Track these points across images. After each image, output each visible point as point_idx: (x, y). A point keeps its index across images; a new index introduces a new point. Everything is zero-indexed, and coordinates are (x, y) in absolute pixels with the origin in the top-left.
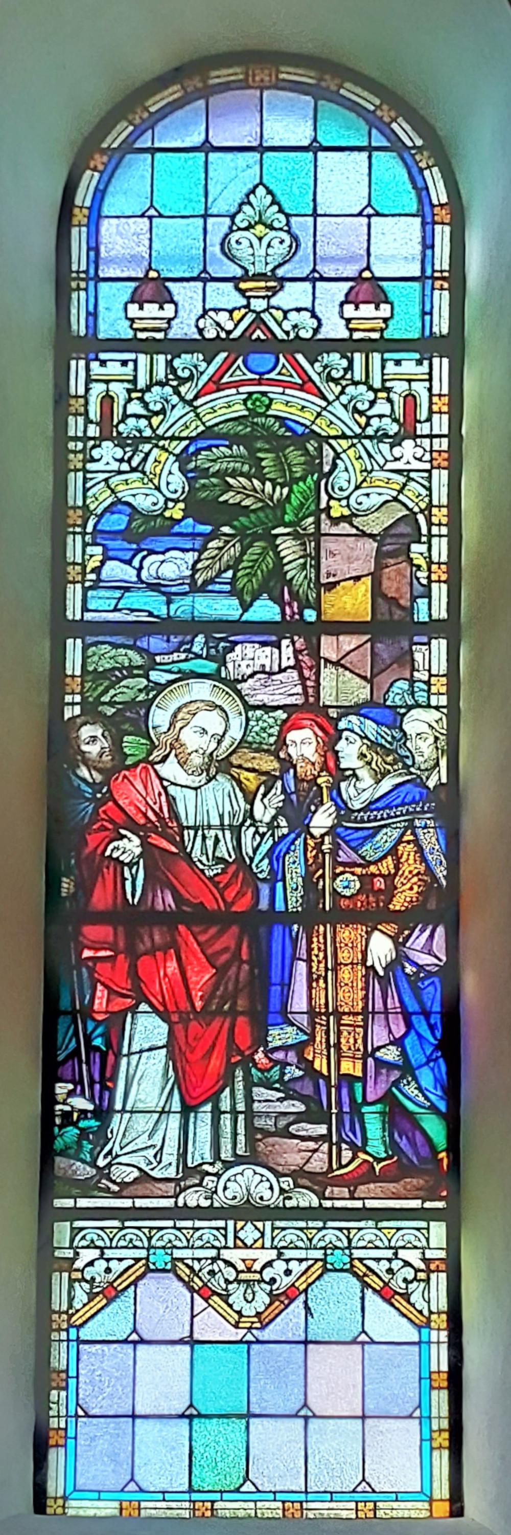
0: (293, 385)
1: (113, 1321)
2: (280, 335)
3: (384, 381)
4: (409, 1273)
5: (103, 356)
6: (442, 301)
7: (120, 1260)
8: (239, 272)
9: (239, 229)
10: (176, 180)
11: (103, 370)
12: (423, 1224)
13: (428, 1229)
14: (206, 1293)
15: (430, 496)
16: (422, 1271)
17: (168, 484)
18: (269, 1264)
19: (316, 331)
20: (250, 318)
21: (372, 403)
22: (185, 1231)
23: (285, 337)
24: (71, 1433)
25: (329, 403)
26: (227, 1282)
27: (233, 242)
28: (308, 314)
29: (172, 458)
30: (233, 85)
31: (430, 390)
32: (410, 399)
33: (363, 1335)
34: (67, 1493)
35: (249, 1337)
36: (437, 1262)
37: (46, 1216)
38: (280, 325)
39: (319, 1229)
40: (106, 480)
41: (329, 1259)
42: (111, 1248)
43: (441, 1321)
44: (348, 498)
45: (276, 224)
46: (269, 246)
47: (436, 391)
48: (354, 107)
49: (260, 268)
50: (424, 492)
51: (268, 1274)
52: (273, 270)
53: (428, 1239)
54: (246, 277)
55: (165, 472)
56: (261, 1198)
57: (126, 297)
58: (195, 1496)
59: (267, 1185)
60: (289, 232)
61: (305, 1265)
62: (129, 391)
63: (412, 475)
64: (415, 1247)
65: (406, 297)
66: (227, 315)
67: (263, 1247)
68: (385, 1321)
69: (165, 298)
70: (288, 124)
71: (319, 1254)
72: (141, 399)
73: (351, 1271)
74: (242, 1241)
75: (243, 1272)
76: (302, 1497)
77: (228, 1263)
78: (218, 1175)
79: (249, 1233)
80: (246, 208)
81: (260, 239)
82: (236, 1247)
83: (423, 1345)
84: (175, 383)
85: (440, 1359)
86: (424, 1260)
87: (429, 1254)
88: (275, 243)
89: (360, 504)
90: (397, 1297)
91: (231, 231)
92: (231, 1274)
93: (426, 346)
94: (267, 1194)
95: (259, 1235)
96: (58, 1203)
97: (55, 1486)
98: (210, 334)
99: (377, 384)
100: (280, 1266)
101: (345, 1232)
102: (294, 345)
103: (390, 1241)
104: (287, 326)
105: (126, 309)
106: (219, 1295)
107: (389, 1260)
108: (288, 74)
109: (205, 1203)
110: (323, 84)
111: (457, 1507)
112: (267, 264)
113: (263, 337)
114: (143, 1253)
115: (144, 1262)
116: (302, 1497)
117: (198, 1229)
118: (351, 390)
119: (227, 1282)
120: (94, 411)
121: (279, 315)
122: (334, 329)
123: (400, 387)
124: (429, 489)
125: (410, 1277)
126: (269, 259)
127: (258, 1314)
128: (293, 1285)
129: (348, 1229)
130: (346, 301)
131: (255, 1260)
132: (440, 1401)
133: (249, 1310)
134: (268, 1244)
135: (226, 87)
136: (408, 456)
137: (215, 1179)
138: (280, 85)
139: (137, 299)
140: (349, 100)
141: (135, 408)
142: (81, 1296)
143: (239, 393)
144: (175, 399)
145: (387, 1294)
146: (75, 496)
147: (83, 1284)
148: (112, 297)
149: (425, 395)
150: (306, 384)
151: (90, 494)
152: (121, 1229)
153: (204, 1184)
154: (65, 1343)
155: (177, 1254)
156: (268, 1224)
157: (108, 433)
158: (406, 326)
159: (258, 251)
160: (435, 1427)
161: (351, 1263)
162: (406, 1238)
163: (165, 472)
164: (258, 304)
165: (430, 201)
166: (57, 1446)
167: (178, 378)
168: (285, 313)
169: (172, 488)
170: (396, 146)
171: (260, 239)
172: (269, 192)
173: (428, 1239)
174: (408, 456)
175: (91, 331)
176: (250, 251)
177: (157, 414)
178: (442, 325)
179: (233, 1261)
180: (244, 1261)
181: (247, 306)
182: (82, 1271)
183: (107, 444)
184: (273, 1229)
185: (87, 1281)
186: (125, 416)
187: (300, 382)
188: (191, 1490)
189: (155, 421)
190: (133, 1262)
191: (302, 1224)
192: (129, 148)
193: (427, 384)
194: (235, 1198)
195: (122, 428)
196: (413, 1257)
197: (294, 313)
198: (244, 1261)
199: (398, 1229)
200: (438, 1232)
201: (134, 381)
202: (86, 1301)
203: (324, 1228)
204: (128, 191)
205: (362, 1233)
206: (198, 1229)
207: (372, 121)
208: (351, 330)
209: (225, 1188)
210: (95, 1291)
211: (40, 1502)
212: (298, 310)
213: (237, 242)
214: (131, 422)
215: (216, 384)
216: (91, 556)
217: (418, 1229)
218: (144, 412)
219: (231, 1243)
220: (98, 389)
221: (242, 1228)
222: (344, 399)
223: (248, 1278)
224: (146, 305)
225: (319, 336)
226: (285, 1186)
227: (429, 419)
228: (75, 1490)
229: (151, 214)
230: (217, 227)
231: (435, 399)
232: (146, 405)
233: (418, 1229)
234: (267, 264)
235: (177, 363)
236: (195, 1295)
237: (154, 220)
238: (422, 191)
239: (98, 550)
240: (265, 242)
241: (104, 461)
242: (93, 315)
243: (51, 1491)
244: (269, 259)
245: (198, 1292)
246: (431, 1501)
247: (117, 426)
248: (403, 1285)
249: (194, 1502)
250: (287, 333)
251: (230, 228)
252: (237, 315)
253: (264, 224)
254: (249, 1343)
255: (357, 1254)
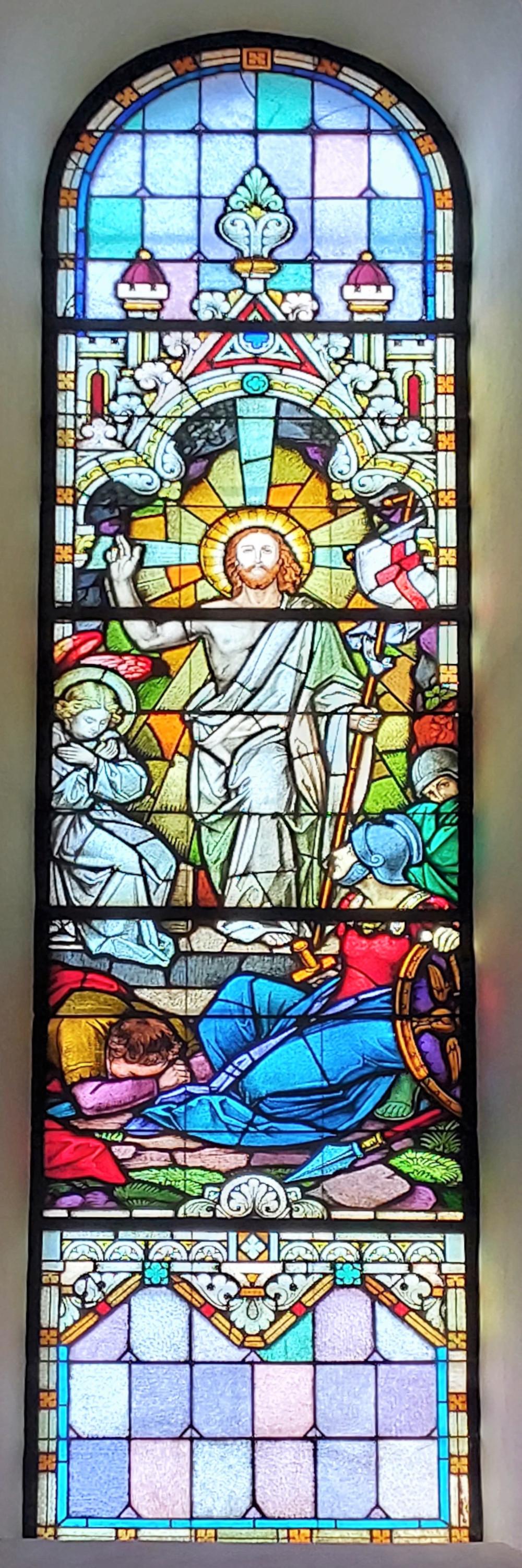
0: (291, 365)
1: (107, 1336)
2: (280, 317)
3: (386, 361)
4: (425, 1290)
5: (92, 334)
6: (445, 284)
7: (115, 1273)
8: (230, 254)
9: (233, 210)
10: (171, 161)
11: (92, 347)
12: (438, 1237)
13: (443, 1242)
14: (208, 1311)
15: (436, 479)
16: (439, 1287)
17: (163, 464)
18: (274, 1279)
19: (316, 313)
20: (247, 298)
21: (375, 384)
22: (184, 1243)
23: (283, 318)
24: (63, 1456)
25: (328, 384)
26: (227, 1296)
27: (228, 225)
28: (308, 296)
29: (166, 438)
30: (225, 68)
31: (435, 370)
32: (415, 382)
33: (375, 1355)
34: (59, 1521)
35: (253, 1357)
36: (455, 1278)
37: (38, 1226)
38: (279, 308)
39: (329, 1242)
40: (97, 459)
41: (338, 1274)
42: (105, 1261)
43: (460, 1340)
44: (350, 480)
45: (272, 206)
46: (266, 227)
47: (441, 371)
48: (350, 91)
49: (256, 249)
50: (431, 475)
51: (272, 1289)
52: (272, 251)
53: (444, 1252)
54: (242, 258)
55: (161, 451)
56: (268, 1209)
57: (118, 276)
58: (196, 1523)
59: (274, 1195)
60: (286, 213)
61: (311, 1280)
62: (121, 369)
63: (415, 457)
64: (430, 1262)
65: (408, 280)
66: (223, 296)
67: (268, 1261)
68: (398, 1340)
69: (381, 279)
70: (287, 101)
71: (325, 1268)
72: (132, 377)
73: (363, 1287)
74: (245, 1254)
75: (245, 1287)
76: (313, 1524)
77: (230, 1278)
78: (220, 1185)
79: (253, 1246)
80: (241, 190)
81: (256, 222)
82: (238, 1261)
83: (440, 1364)
84: (168, 361)
85: (458, 1380)
86: (440, 1274)
87: (445, 1268)
88: (272, 224)
89: (363, 486)
90: (412, 1314)
91: (225, 213)
92: (233, 1289)
93: (428, 328)
94: (274, 1205)
95: (262, 1247)
96: (49, 1214)
97: (46, 1512)
98: (205, 315)
99: (380, 365)
100: (285, 1280)
101: (356, 1245)
102: (288, 328)
103: (404, 1255)
104: (286, 308)
105: (116, 288)
106: (221, 1312)
107: (211, 1274)
108: (283, 57)
109: (205, 1214)
110: (320, 69)
111: (476, 1534)
112: (263, 246)
113: (260, 318)
114: (137, 1267)
115: (138, 1277)
116: (313, 1524)
117: (198, 1241)
118: (350, 368)
119: (420, 1296)
120: (84, 391)
121: (278, 297)
122: (334, 311)
123: (402, 370)
124: (435, 472)
125: (233, 1294)
126: (265, 241)
127: (261, 1333)
128: (299, 1301)
129: (361, 1243)
130: (123, 280)
131: (259, 1275)
132: (459, 1424)
133: (252, 1329)
134: (274, 1256)
135: (220, 70)
136: (413, 438)
137: (217, 1189)
138: (275, 69)
139: (353, 280)
140: (348, 84)
141: (126, 386)
142: (73, 1313)
143: (233, 373)
144: (168, 377)
145: (399, 1310)
146: (64, 473)
147: (74, 1299)
148: (330, 281)
149: (430, 377)
150: (304, 364)
151: (81, 472)
152: (114, 1241)
153: (206, 1195)
154: (54, 1442)
155: (176, 1267)
156: (274, 1236)
157: (98, 409)
158: (408, 308)
159: (254, 232)
160: (85, 157)
161: (169, 1277)
162: (337, 1252)
163: (161, 451)
164: (255, 286)
165: (432, 185)
166: (47, 1471)
167: (170, 357)
168: (284, 295)
169: (168, 467)
170: (397, 130)
171: (256, 222)
172: (265, 174)
173: (444, 1252)
174: (413, 438)
175: (79, 311)
176: (246, 233)
177: (149, 391)
178: (444, 307)
179: (231, 1273)
180: (246, 1275)
181: (244, 288)
182: (73, 1286)
183: (98, 422)
184: (280, 1240)
185: (78, 1296)
186: (115, 397)
187: (297, 361)
188: (192, 1518)
189: (148, 399)
190: (128, 1275)
191: (308, 1236)
192: (117, 129)
193: (431, 364)
194: (239, 1209)
195: (113, 406)
196: (429, 1271)
197: (294, 295)
198: (246, 1275)
199: (413, 1242)
200: (456, 1244)
201: (125, 360)
202: (77, 1318)
203: (335, 1241)
204: (119, 167)
205: (374, 1246)
206: (198, 1241)
207: (370, 104)
208: (127, 311)
209: (230, 1198)
210: (88, 1306)
211: (30, 1527)
212: (298, 292)
213: (233, 224)
214: (123, 400)
215: (209, 363)
216: (82, 536)
217: (434, 1242)
218: (136, 390)
219: (233, 1257)
220: (87, 367)
221: (246, 1240)
222: (345, 378)
223: (253, 1293)
224: (363, 288)
225: (319, 318)
226: (292, 1197)
227: (435, 402)
228: (68, 1516)
229: (143, 194)
230: (212, 208)
231: (440, 380)
232: (137, 383)
233: (434, 1242)
234: (263, 246)
235: (167, 340)
236: (195, 1313)
237: (257, 1367)
238: (423, 176)
239: (91, 529)
240: (261, 224)
241: (408, 442)
242: (81, 293)
243: (41, 1518)
244: (265, 241)
245: (198, 1309)
246: (450, 1527)
247: (108, 406)
248: (419, 1302)
249: (196, 1529)
250: (286, 315)
251: (225, 209)
252: (233, 296)
253: (260, 206)
254: (252, 1363)
255: (369, 1269)
